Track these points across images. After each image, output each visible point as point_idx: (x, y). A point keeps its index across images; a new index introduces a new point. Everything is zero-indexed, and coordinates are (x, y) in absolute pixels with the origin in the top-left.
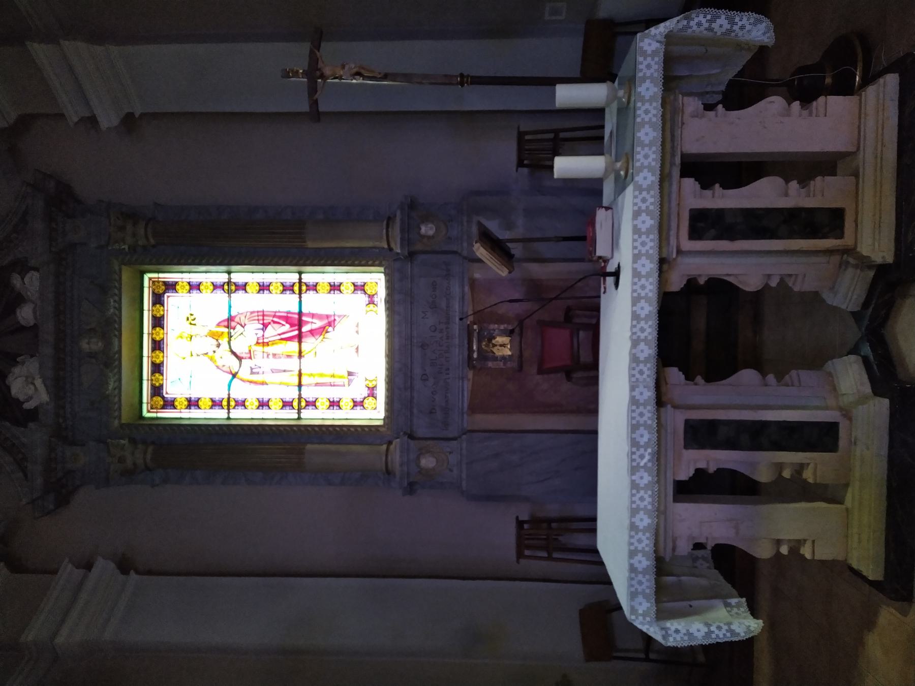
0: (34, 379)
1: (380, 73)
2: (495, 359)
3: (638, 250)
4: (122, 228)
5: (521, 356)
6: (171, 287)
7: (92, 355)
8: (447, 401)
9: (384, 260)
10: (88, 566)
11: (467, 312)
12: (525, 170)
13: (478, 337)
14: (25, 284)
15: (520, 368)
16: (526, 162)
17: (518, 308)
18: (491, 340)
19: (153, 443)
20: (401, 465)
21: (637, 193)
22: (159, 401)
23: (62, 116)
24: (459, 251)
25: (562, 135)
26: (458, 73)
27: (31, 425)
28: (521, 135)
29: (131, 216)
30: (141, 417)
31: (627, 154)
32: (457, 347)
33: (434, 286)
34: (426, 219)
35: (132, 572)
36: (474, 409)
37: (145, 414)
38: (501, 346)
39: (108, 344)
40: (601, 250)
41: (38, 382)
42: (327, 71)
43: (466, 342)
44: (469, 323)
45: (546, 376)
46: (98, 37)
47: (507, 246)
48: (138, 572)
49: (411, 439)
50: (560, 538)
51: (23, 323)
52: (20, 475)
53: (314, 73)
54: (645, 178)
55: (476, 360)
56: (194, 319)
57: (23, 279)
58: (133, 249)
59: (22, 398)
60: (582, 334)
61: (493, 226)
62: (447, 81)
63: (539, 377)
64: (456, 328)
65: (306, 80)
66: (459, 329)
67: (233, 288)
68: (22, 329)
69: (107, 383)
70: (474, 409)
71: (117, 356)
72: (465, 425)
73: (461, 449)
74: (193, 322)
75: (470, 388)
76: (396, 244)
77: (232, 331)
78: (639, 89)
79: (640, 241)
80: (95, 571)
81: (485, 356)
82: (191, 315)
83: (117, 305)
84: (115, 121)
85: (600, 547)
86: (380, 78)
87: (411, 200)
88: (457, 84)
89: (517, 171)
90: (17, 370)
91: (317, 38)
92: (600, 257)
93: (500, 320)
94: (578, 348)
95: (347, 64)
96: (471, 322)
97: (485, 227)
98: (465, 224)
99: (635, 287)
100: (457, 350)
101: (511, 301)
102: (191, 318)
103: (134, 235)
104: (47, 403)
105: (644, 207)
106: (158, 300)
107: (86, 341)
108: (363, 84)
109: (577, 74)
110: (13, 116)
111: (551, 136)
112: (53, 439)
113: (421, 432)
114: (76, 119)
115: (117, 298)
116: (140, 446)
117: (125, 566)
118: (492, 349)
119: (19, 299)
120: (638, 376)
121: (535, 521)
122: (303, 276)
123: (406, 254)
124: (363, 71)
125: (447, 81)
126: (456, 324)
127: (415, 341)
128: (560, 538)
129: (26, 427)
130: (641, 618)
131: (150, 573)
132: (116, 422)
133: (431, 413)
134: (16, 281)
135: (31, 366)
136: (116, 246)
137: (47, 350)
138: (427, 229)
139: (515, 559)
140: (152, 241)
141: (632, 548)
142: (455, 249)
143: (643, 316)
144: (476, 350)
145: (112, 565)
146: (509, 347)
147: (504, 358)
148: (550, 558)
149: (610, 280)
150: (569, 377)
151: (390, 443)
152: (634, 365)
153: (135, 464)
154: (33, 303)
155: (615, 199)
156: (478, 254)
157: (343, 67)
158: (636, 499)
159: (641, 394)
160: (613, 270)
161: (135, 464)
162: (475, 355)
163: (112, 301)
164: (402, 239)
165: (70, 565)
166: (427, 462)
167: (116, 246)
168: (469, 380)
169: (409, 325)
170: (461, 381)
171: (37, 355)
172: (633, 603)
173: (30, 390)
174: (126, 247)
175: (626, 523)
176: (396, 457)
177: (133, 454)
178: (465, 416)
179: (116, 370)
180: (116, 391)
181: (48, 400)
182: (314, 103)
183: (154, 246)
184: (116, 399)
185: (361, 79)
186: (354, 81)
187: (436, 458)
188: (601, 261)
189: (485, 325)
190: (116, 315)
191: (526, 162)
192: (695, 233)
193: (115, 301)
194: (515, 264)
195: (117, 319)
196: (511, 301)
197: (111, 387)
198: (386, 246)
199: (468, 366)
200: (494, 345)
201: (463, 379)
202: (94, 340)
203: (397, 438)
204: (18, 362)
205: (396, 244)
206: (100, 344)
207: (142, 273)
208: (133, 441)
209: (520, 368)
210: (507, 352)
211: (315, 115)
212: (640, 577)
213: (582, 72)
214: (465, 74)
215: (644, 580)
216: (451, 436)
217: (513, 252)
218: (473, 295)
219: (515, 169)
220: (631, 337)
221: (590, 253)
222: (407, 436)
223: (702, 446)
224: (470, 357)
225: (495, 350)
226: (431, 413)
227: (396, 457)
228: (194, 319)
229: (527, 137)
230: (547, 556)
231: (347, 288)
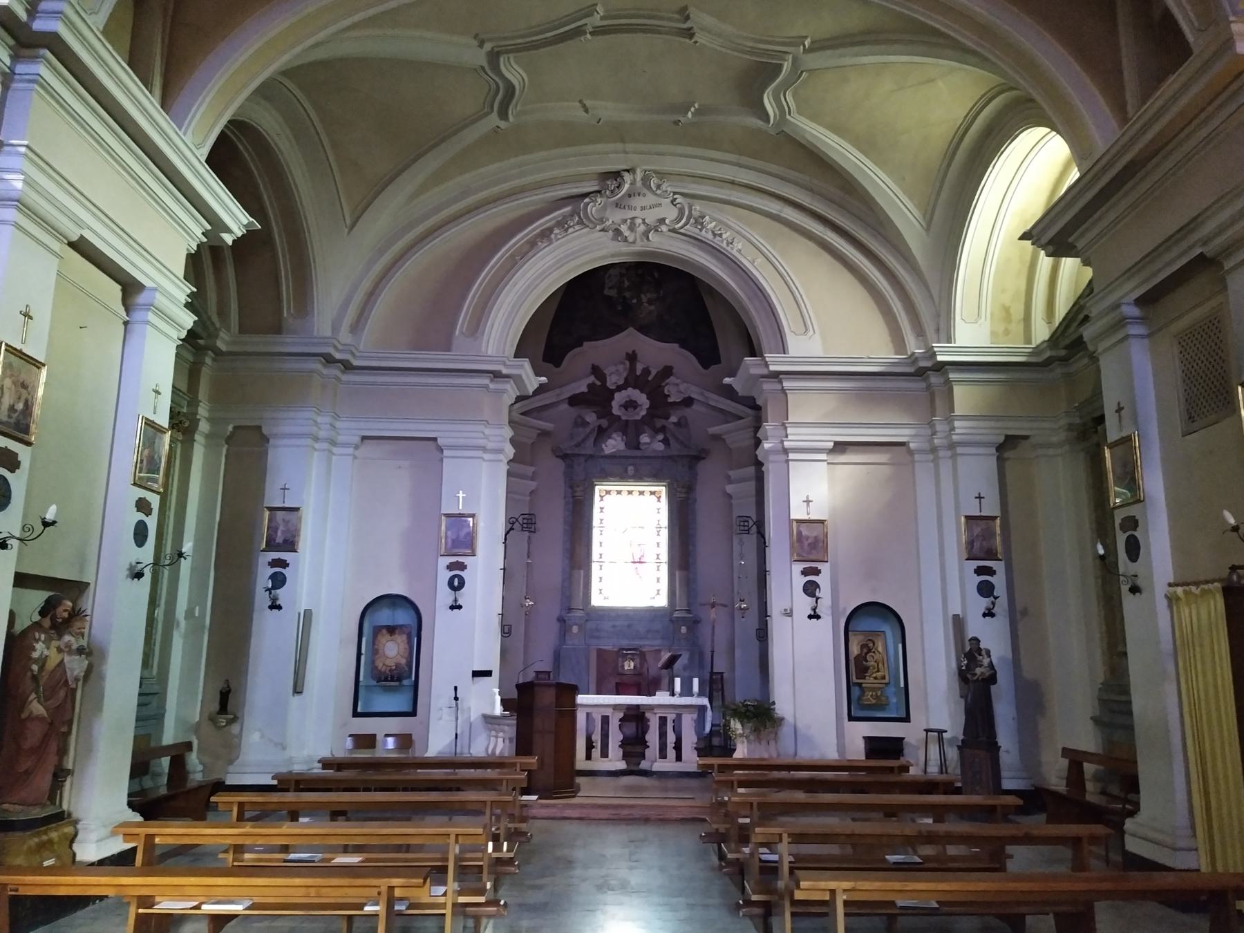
2: (623, 662)
4: (683, 487)
7: (626, 471)
34: (688, 629)
41: (614, 450)
59: (607, 443)
64: (637, 643)
70: (601, 653)
80: (531, 482)
81: (625, 657)
106: (652, 493)
110: (731, 446)
135: (622, 446)
138: (684, 629)
145: (533, 488)
147: (623, 666)
166: (575, 629)
192: (660, 718)
223: (602, 720)
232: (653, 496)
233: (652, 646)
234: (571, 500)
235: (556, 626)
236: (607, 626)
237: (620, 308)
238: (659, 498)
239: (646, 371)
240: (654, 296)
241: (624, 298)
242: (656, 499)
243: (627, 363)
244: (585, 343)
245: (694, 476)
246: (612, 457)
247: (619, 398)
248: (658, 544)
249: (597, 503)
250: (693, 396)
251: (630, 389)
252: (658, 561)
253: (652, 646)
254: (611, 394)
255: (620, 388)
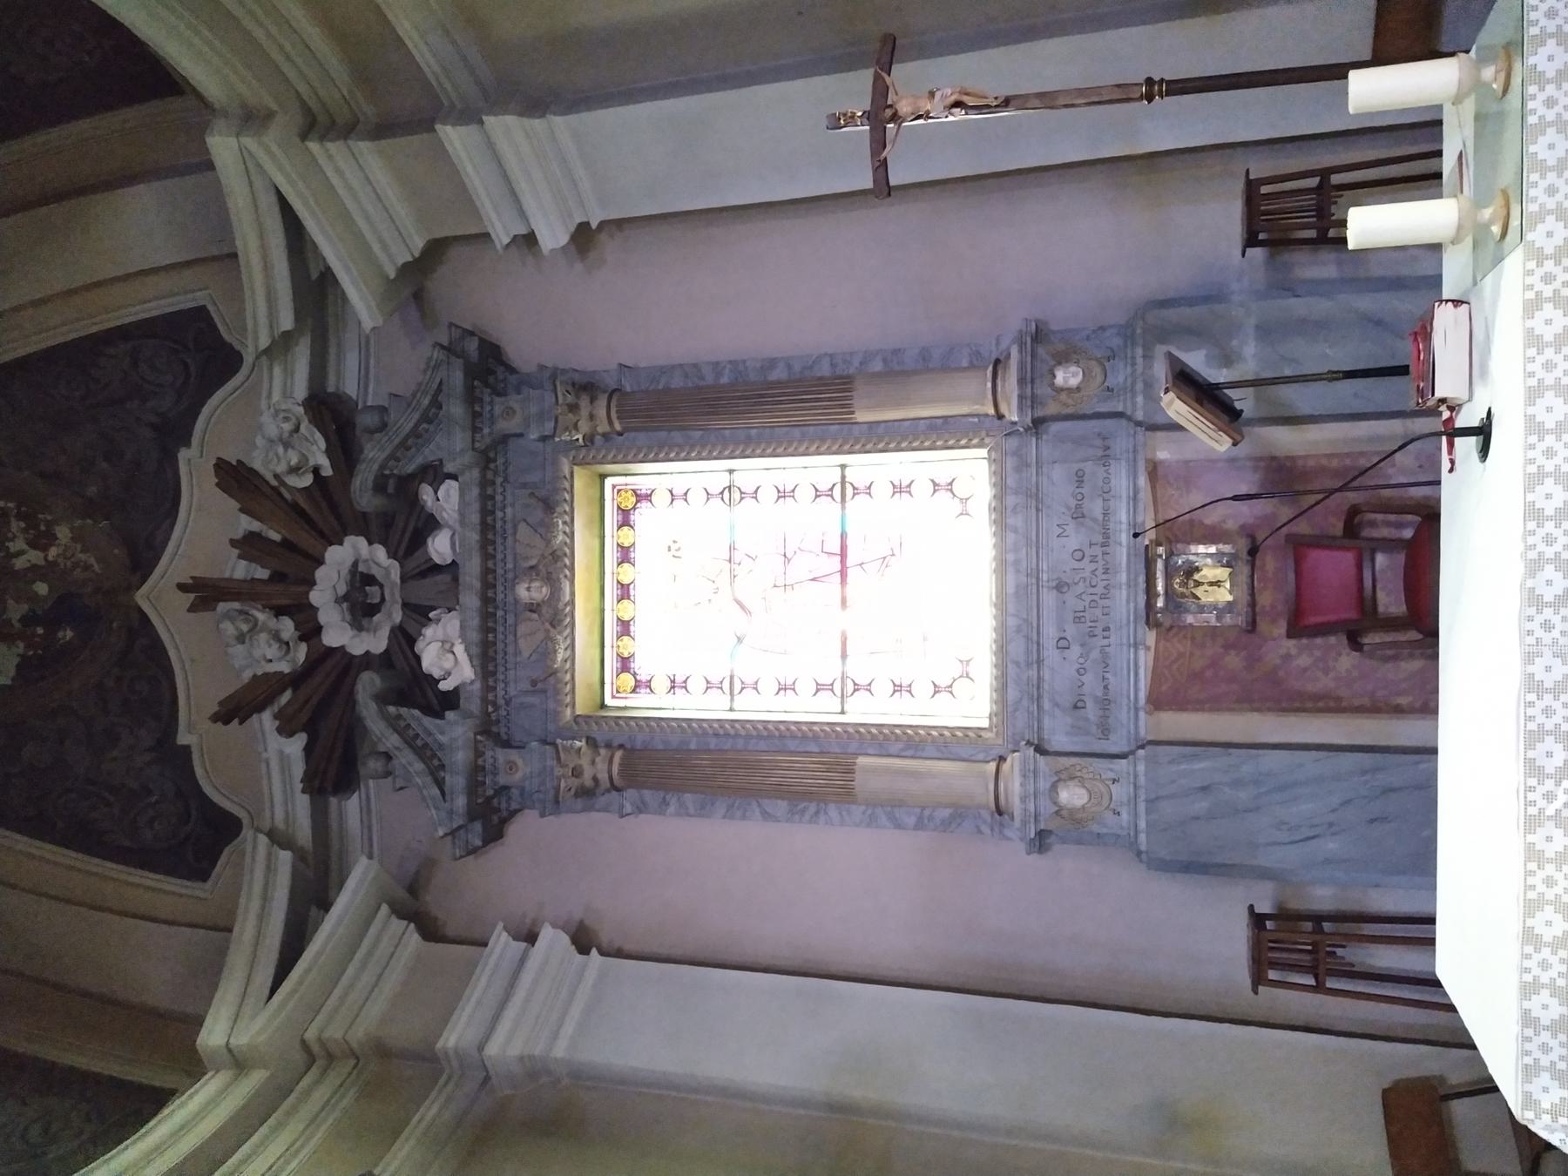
0: (453, 645)
1: (996, 98)
2: (1202, 609)
3: (1536, 379)
4: (573, 408)
5: (1253, 604)
6: (642, 497)
7: (533, 608)
8: (1106, 687)
9: (988, 435)
10: (531, 938)
11: (1143, 523)
12: (1257, 253)
13: (1166, 567)
14: (438, 500)
15: (1252, 626)
16: (1261, 236)
17: (1246, 512)
18: (1192, 575)
19: (621, 746)
20: (1024, 799)
21: (1532, 265)
22: (627, 680)
23: (487, 235)
24: (1129, 413)
25: (1336, 179)
26: (1141, 80)
27: (450, 715)
28: (1251, 187)
29: (587, 387)
30: (603, 706)
31: (1505, 193)
32: (1124, 587)
33: (1080, 479)
34: (1062, 359)
35: (594, 951)
36: (1158, 702)
37: (609, 701)
38: (1212, 584)
39: (556, 591)
40: (1447, 384)
41: (459, 649)
42: (904, 108)
43: (1142, 579)
44: (1147, 543)
45: (1305, 641)
46: (536, 105)
47: (1225, 394)
48: (602, 953)
49: (1041, 755)
50: (1339, 951)
51: (438, 560)
52: (436, 791)
53: (881, 115)
54: (1550, 234)
55: (1162, 610)
56: (678, 550)
57: (436, 492)
58: (590, 439)
59: (436, 674)
60: (1380, 559)
61: (1196, 360)
62: (1122, 94)
63: (1292, 642)
64: (1122, 550)
65: (868, 128)
66: (1129, 555)
67: (737, 495)
68: (436, 569)
69: (555, 651)
70: (1158, 702)
71: (568, 609)
72: (1142, 732)
73: (1136, 776)
74: (677, 554)
75: (1151, 663)
76: (1009, 405)
77: (736, 566)
78: (1531, 60)
79: (1540, 359)
80: (541, 942)
82: (675, 542)
83: (567, 530)
84: (564, 239)
85: (1442, 973)
86: (996, 106)
87: (1037, 326)
88: (1141, 98)
89: (1243, 255)
90: (429, 632)
91: (887, 53)
92: (1443, 401)
93: (1211, 536)
94: (1374, 587)
95: (938, 90)
96: (1151, 541)
97: (1178, 359)
98: (1139, 361)
99: (1531, 454)
100: (1124, 593)
101: (1235, 498)
102: (674, 547)
103: (592, 417)
104: (472, 682)
105: (1548, 291)
106: (625, 520)
107: (526, 586)
108: (966, 121)
109: (1367, 55)
110: (419, 244)
111: (1313, 182)
112: (479, 737)
113: (1059, 739)
114: (506, 240)
115: (567, 518)
116: (603, 751)
117: (583, 941)
118: (1193, 590)
119: (431, 524)
120: (1539, 633)
121: (1286, 916)
122: (848, 471)
123: (1028, 420)
124: (965, 99)
125: (1122, 94)
126: (1120, 544)
127: (1045, 578)
128: (1339, 951)
129: (442, 717)
130: (1547, 1118)
131: (620, 954)
132: (568, 711)
133: (1076, 707)
134: (426, 493)
136: (566, 437)
137: (470, 600)
138: (1068, 376)
139: (1248, 982)
140: (618, 427)
141: (1528, 978)
142: (1120, 409)
143: (1549, 511)
144: (1162, 592)
145: (566, 939)
146: (1228, 585)
148: (1319, 988)
149: (1467, 446)
150: (1355, 642)
151: (1002, 759)
152: (1532, 611)
153: (595, 779)
154: (450, 527)
155: (1475, 283)
156: (1171, 414)
157: (932, 94)
158: (1536, 880)
159: (1548, 669)
160: (1475, 422)
161: (595, 779)
162: (1160, 603)
163: (560, 522)
164: (1021, 397)
165: (505, 934)
166: (1073, 796)
167: (566, 437)
168: (1148, 648)
169: (1034, 549)
170: (1132, 650)
171: (457, 607)
172: (1528, 1087)
173: (448, 663)
174: (580, 436)
175: (1515, 928)
176: (1014, 785)
177: (593, 762)
178: (1142, 714)
179: (568, 631)
180: (568, 665)
181: (473, 677)
182: (881, 168)
183: (620, 434)
184: (568, 677)
185: (963, 112)
186: (951, 118)
187: (1088, 790)
188: (1443, 408)
189: (1179, 546)
190: (566, 543)
191: (1261, 236)
193: (565, 523)
194: (1245, 430)
195: (567, 551)
196: (1235, 498)
197: (560, 657)
198: (992, 411)
199: (1147, 623)
200: (1198, 584)
201: (1136, 645)
202: (536, 584)
203: (1014, 751)
204: (430, 620)
205: (1009, 405)
206: (544, 590)
207: (603, 477)
208: (592, 743)
209: (1252, 626)
210: (1224, 595)
211: (883, 189)
212: (1545, 1036)
213: (1375, 51)
214: (1157, 79)
215: (1553, 1043)
216: (1114, 750)
217: (1238, 405)
218: (1153, 488)
219: (1239, 252)
220: (1524, 555)
221: (1421, 393)
222: (1032, 749)
224: (1150, 605)
225: (1199, 592)
226: (1076, 707)
227: (1014, 785)
228: (678, 550)
229: (1264, 190)
230: (1314, 984)
231: (922, 488)
232: (636, 517)
233: (1135, 498)
234: (631, 793)
235: (1066, 862)
236: (1060, 671)
237: (67, 634)
238: (642, 497)
239: (249, 545)
240: (16, 525)
241: (27, 620)
242: (644, 505)
243: (222, 607)
244: (183, 738)
245: (554, 376)
246: (488, 657)
247: (336, 634)
248: (782, 495)
249: (645, 705)
250: (301, 391)
251: (315, 597)
252: (837, 492)
253: (1135, 498)
254: (323, 657)
255: (310, 631)
